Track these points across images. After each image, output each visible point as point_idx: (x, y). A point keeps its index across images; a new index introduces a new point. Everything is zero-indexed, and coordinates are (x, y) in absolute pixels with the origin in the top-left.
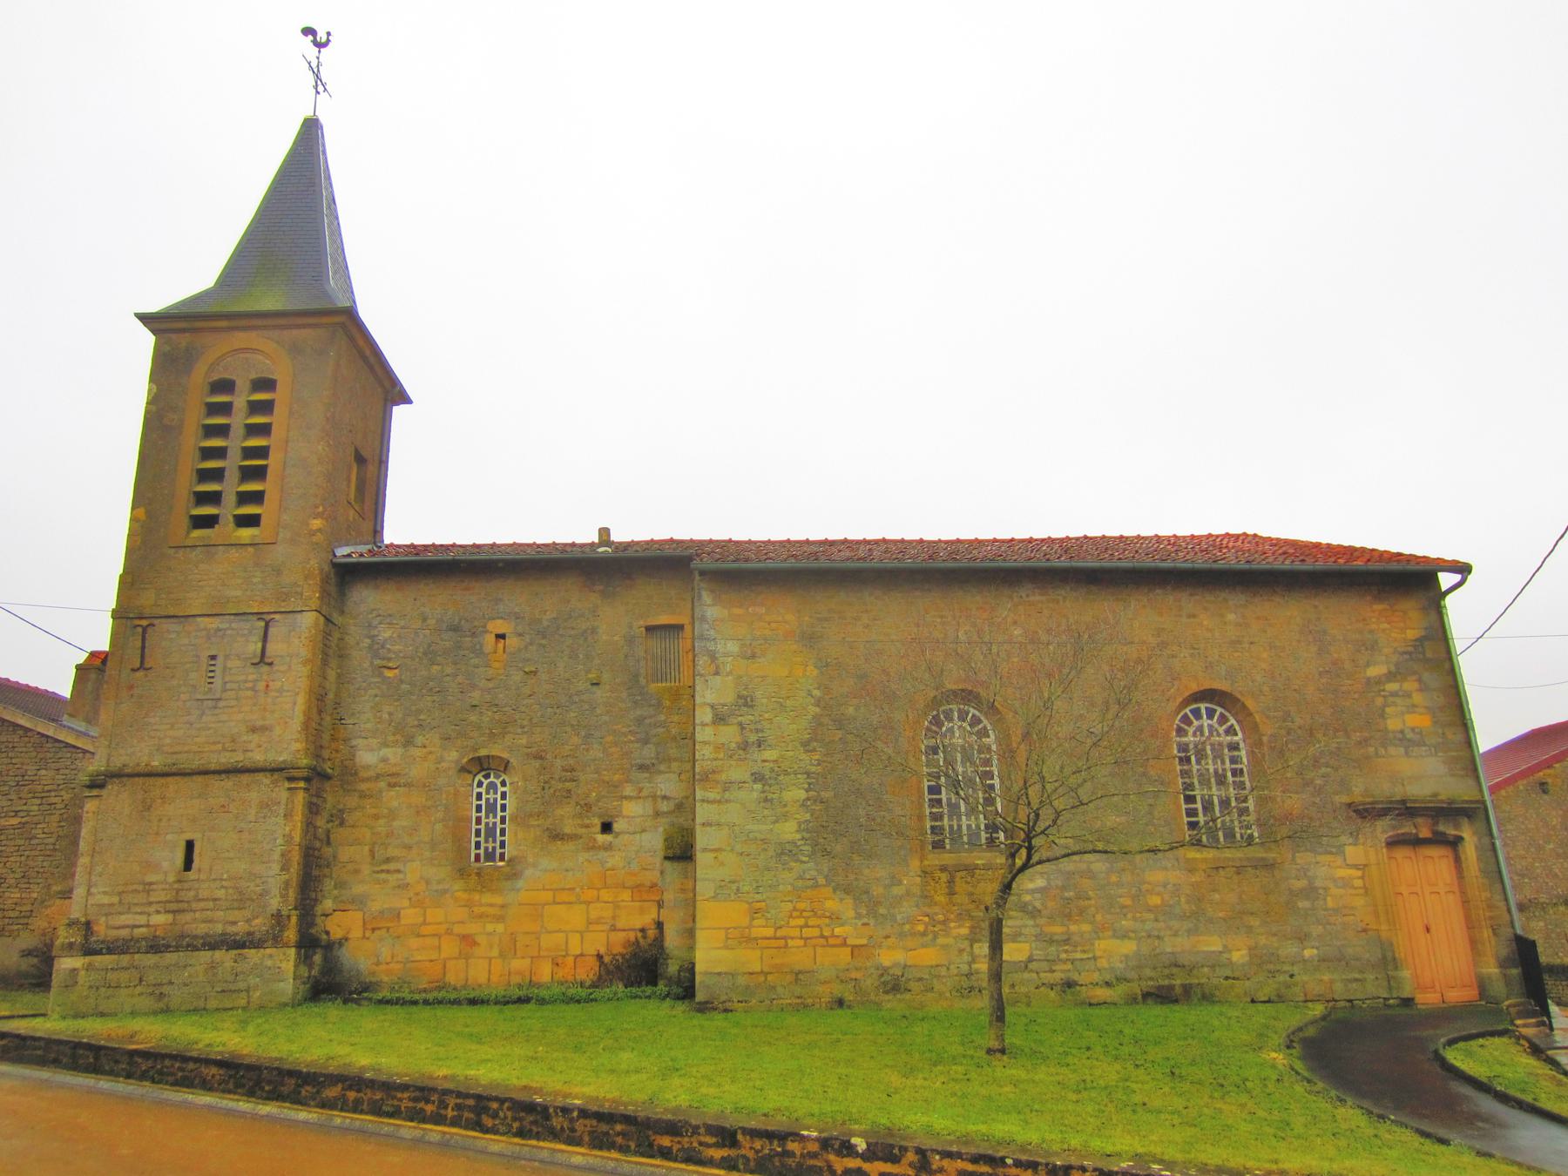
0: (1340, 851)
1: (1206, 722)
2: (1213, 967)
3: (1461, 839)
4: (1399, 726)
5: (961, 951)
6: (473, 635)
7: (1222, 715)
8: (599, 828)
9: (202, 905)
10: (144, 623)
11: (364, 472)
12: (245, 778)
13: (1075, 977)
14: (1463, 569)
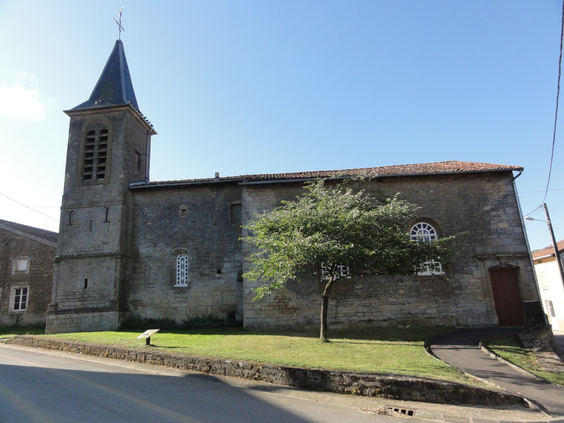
0: (471, 273)
1: (422, 229)
2: (423, 314)
3: (518, 268)
4: (496, 227)
5: (333, 309)
6: (175, 210)
7: (423, 225)
8: (216, 272)
9: (90, 299)
10: (70, 210)
11: (140, 159)
12: (102, 259)
13: (372, 318)
14: (521, 169)
